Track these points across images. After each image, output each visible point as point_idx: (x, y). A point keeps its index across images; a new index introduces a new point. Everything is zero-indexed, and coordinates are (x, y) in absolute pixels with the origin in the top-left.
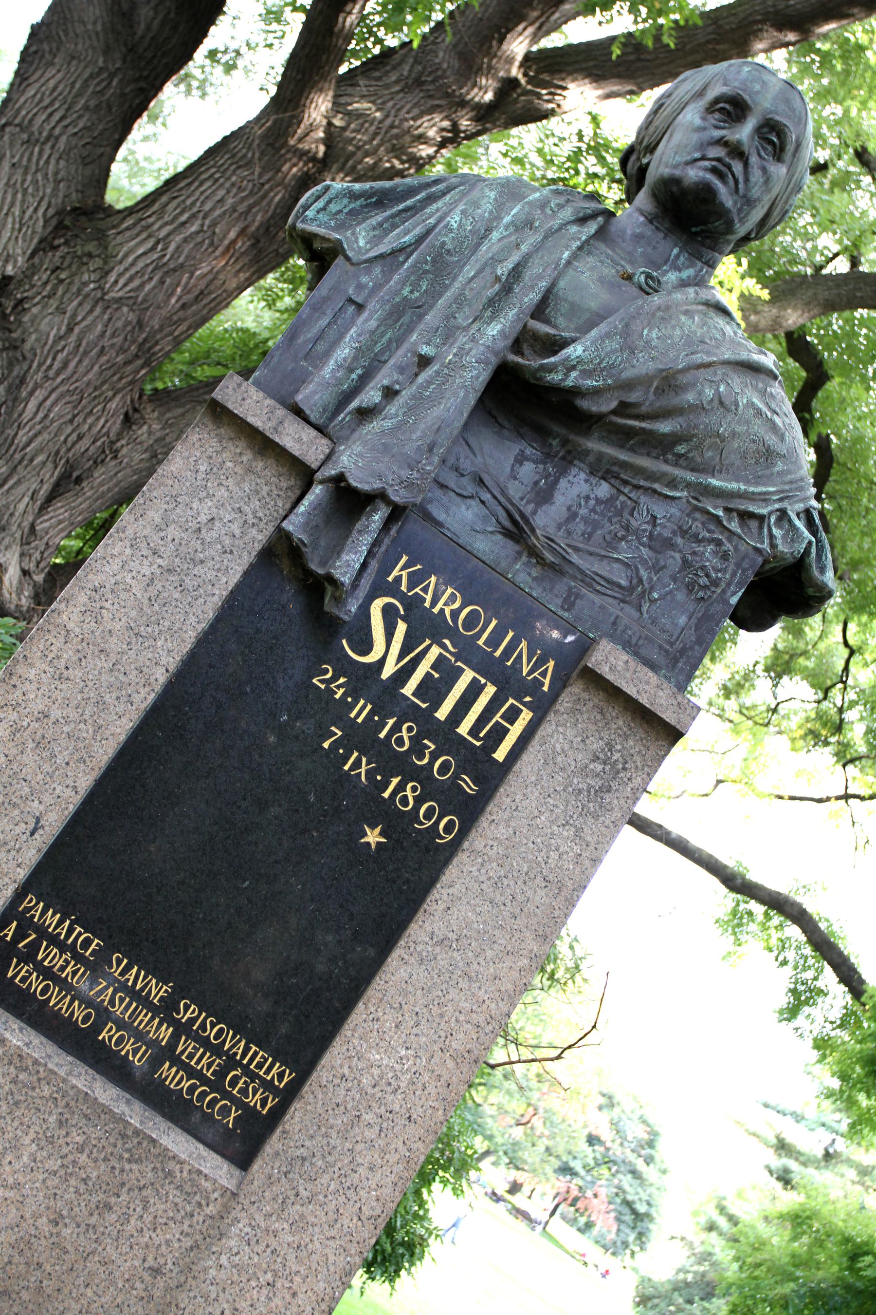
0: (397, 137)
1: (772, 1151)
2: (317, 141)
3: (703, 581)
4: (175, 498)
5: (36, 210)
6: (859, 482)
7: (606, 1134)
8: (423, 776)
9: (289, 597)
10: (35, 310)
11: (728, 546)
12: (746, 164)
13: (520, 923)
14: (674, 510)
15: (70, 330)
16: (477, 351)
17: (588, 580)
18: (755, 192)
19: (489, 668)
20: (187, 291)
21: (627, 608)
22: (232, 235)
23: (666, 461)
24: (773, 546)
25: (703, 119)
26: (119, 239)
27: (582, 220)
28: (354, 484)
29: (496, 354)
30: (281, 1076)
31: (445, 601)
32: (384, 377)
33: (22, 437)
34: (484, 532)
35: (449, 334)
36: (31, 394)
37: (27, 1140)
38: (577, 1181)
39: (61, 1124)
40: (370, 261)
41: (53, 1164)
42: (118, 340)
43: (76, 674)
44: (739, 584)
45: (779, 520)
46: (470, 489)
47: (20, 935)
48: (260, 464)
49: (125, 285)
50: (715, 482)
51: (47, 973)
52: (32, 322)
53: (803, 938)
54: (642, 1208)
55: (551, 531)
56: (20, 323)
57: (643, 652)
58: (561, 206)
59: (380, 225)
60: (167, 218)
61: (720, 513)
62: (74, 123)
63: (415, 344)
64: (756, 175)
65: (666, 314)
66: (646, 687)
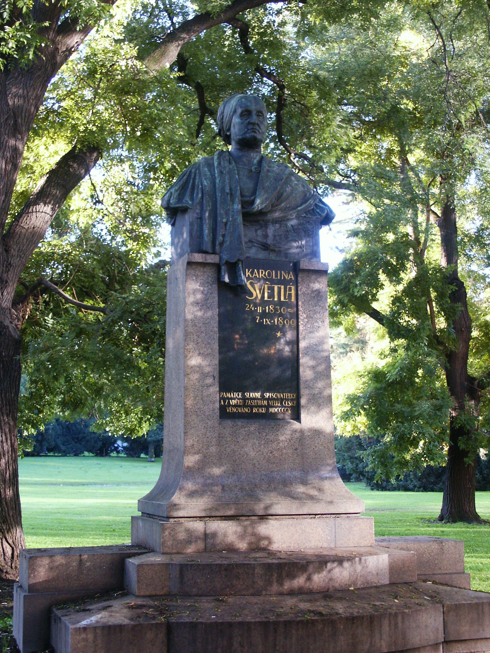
39: (259, 433)
47: (225, 402)
48: (205, 270)
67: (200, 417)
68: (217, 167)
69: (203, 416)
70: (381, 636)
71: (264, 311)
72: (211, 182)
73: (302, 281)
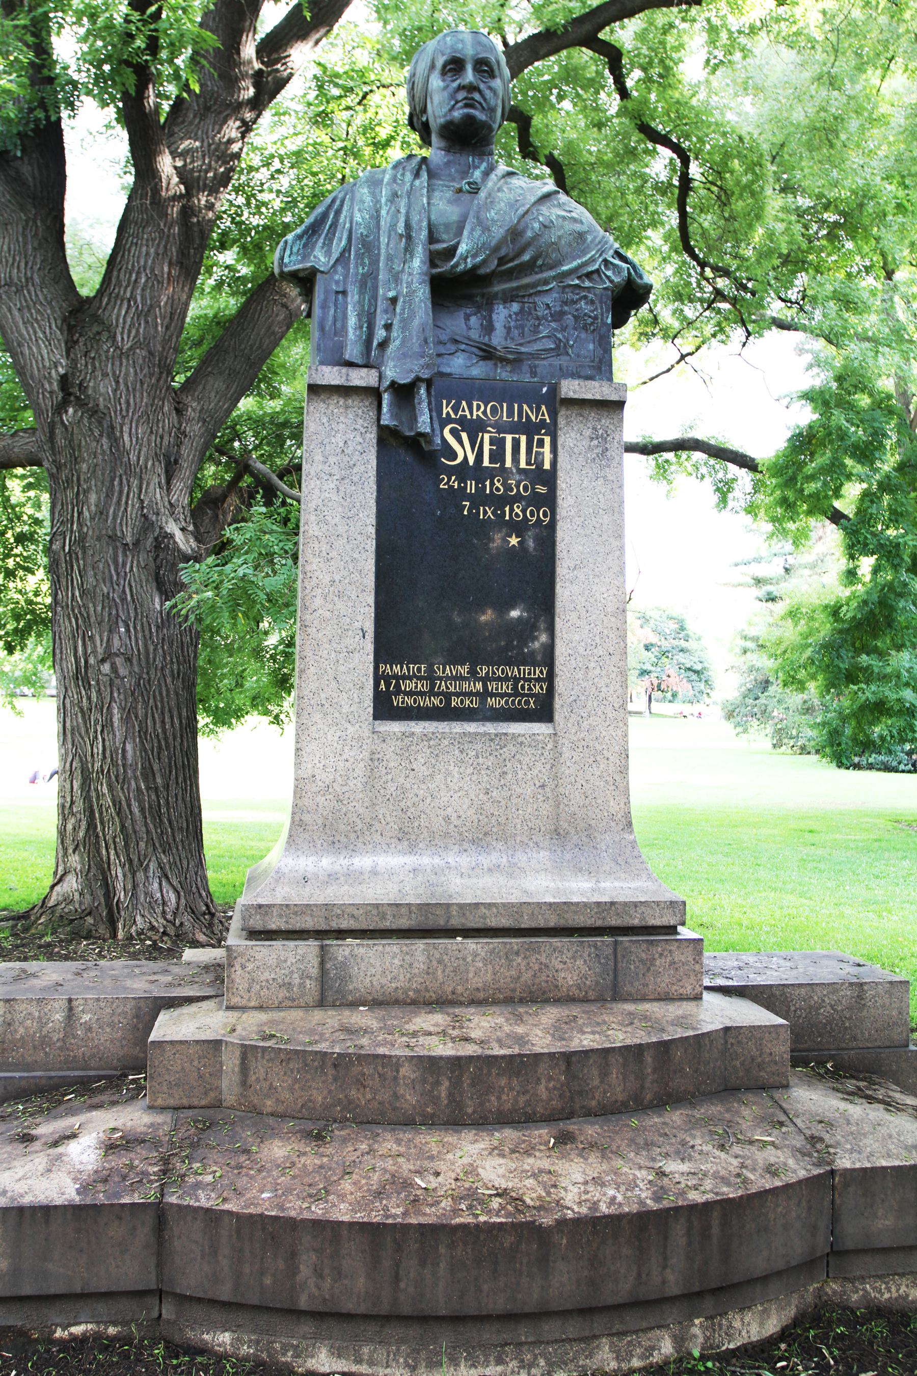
0: (216, 150)
1: (754, 588)
2: (177, 185)
3: (589, 321)
4: (322, 443)
5: (50, 327)
6: (584, 169)
7: (654, 639)
8: (518, 498)
9: (405, 456)
10: (91, 384)
11: (591, 296)
12: (480, 91)
13: (605, 537)
14: (555, 295)
15: (117, 382)
16: (416, 279)
17: (535, 356)
18: (492, 102)
19: (514, 428)
20: (163, 318)
21: (563, 358)
22: (166, 269)
23: (536, 273)
24: (611, 281)
25: (443, 81)
26: (107, 313)
27: (417, 175)
28: (402, 382)
29: (425, 274)
30: (541, 672)
31: (478, 411)
32: (380, 321)
33: (133, 458)
34: (473, 365)
35: (396, 278)
36: (121, 432)
37: (452, 768)
38: (653, 675)
40: (334, 266)
41: (470, 770)
42: (146, 371)
43: (333, 554)
44: (607, 311)
45: (606, 266)
46: (453, 348)
47: (388, 685)
49: (129, 337)
50: (565, 268)
51: (410, 694)
52: (95, 391)
53: (705, 456)
54: (698, 667)
55: (503, 343)
56: (88, 396)
57: (582, 374)
58: (403, 175)
59: (324, 243)
60: (124, 284)
61: (577, 282)
62: (34, 263)
63: (384, 294)
64: (488, 94)
65: (491, 201)
66: (593, 390)
67: (329, 718)
68: (388, 184)
69: (337, 715)
70: (665, 1259)
71: (481, 490)
72: (371, 217)
73: (568, 424)
